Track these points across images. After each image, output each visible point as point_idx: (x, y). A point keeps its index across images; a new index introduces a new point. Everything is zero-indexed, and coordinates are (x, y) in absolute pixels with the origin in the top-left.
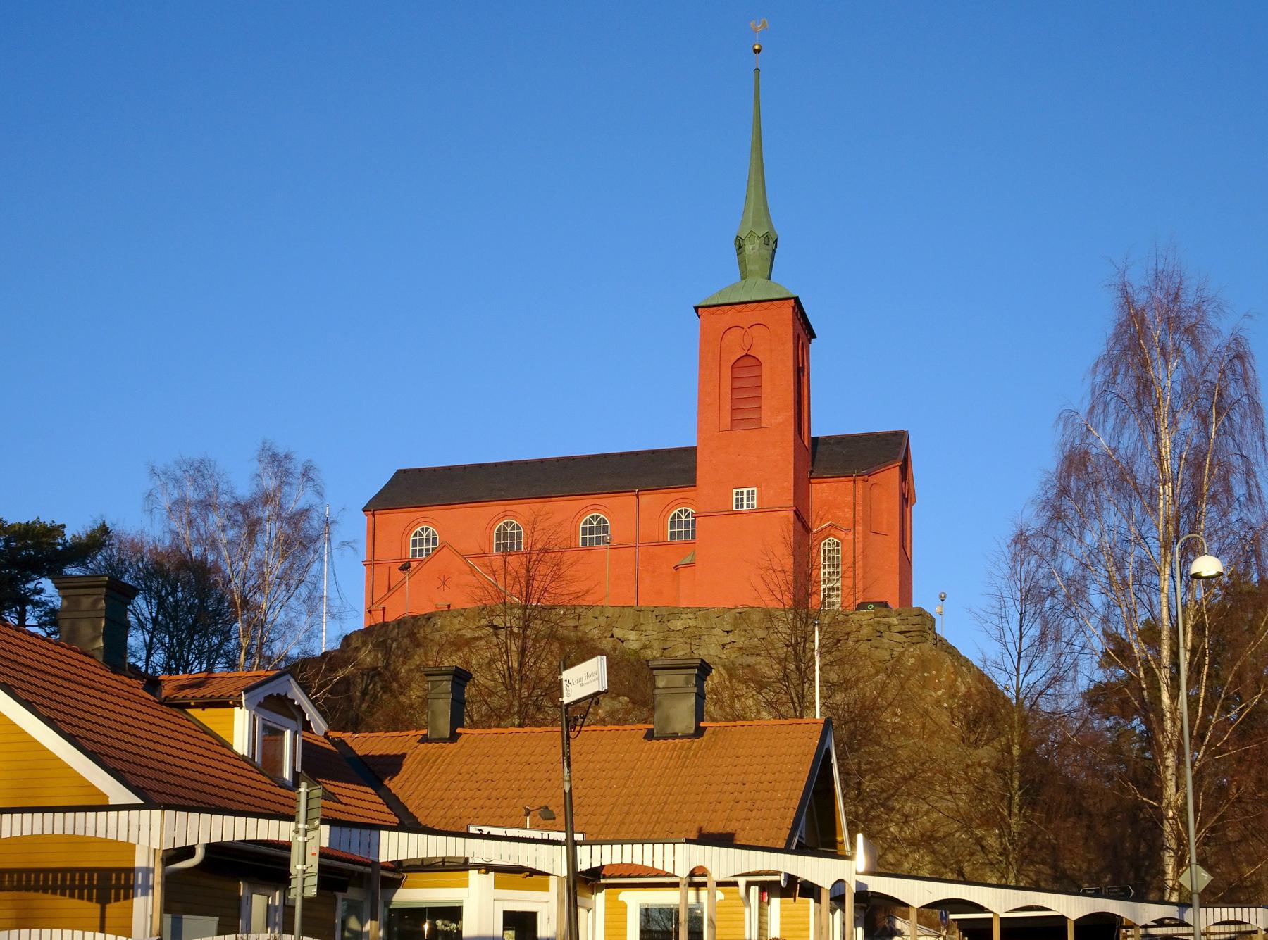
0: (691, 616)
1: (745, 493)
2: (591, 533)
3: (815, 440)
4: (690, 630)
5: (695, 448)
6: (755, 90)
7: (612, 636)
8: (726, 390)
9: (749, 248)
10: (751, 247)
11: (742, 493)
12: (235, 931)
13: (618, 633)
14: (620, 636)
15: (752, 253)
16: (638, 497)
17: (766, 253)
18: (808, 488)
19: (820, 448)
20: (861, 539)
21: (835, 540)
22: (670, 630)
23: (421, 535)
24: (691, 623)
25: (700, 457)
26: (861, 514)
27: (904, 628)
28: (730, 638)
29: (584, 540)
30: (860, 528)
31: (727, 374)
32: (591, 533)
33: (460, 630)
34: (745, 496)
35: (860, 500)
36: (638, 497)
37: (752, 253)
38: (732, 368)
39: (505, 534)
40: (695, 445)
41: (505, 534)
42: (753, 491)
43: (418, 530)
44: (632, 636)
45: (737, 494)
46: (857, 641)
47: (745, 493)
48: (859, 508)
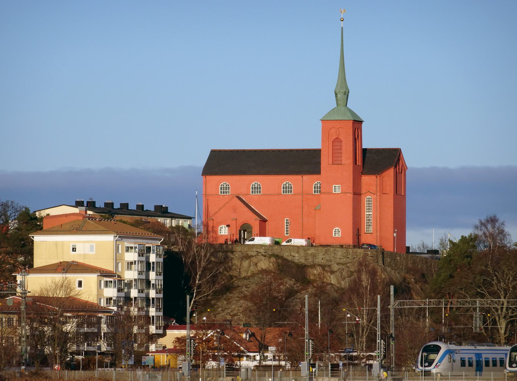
0: (313, 249)
1: (337, 187)
2: (286, 189)
3: (365, 151)
4: (313, 254)
5: (319, 151)
6: (341, 41)
7: (291, 255)
8: (331, 150)
9: (339, 96)
10: (339, 95)
11: (336, 186)
12: (79, 281)
13: (293, 254)
14: (293, 255)
15: (340, 97)
16: (302, 177)
17: (345, 97)
18: (361, 179)
19: (367, 155)
20: (379, 198)
21: (370, 197)
22: (307, 254)
23: (223, 185)
24: (313, 252)
25: (322, 153)
26: (379, 189)
27: (372, 255)
28: (324, 257)
29: (284, 191)
30: (378, 194)
31: (331, 144)
32: (286, 189)
33: (247, 252)
34: (337, 188)
35: (378, 184)
36: (302, 177)
37: (340, 97)
38: (333, 142)
39: (255, 187)
40: (320, 148)
41: (255, 187)
42: (340, 186)
43: (222, 183)
44: (297, 255)
45: (334, 186)
46: (359, 258)
47: (337, 187)
48: (378, 186)
